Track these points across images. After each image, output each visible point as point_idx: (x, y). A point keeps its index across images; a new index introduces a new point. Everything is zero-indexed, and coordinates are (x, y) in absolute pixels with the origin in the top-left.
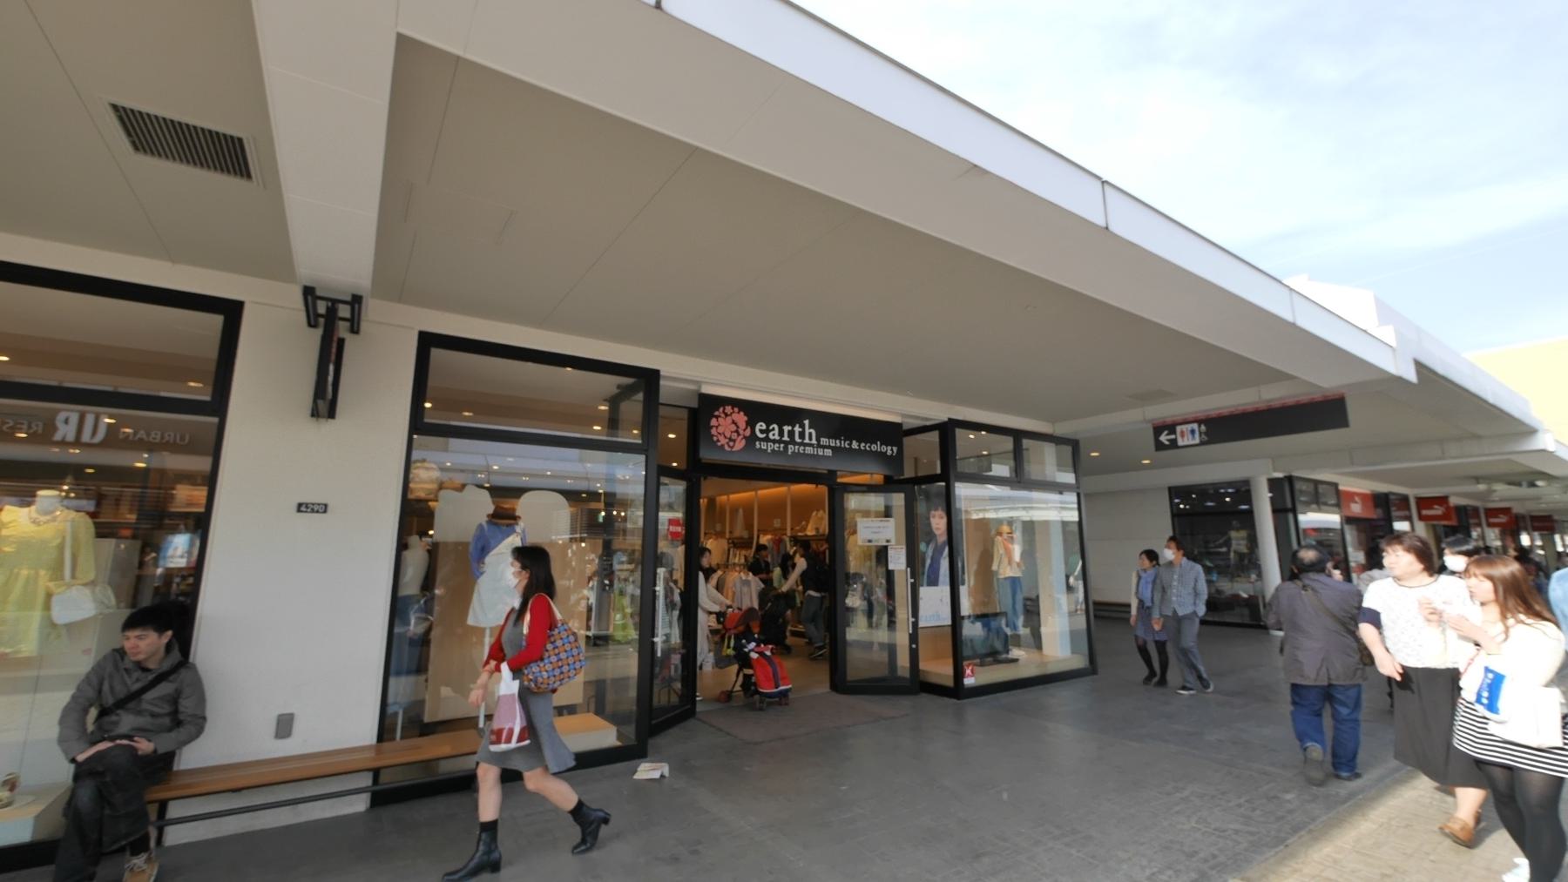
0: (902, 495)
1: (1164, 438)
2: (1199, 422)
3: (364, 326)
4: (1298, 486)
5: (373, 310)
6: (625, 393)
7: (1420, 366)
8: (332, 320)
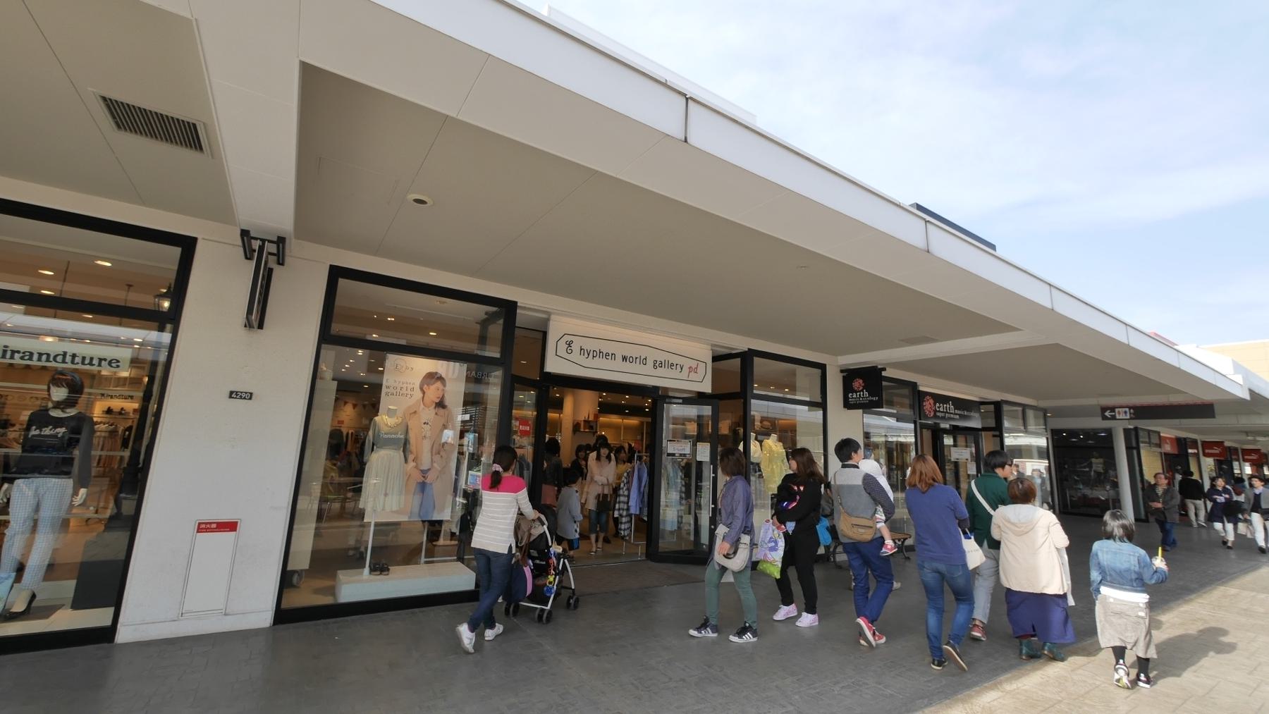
0: (710, 408)
1: (1107, 414)
2: (1130, 408)
3: (287, 260)
4: (1141, 433)
5: (294, 248)
6: (490, 318)
7: (1251, 392)
8: (264, 255)
